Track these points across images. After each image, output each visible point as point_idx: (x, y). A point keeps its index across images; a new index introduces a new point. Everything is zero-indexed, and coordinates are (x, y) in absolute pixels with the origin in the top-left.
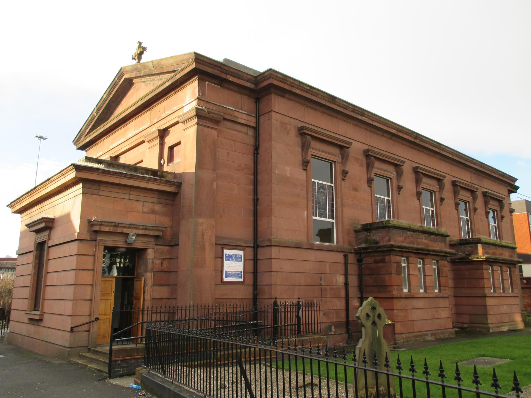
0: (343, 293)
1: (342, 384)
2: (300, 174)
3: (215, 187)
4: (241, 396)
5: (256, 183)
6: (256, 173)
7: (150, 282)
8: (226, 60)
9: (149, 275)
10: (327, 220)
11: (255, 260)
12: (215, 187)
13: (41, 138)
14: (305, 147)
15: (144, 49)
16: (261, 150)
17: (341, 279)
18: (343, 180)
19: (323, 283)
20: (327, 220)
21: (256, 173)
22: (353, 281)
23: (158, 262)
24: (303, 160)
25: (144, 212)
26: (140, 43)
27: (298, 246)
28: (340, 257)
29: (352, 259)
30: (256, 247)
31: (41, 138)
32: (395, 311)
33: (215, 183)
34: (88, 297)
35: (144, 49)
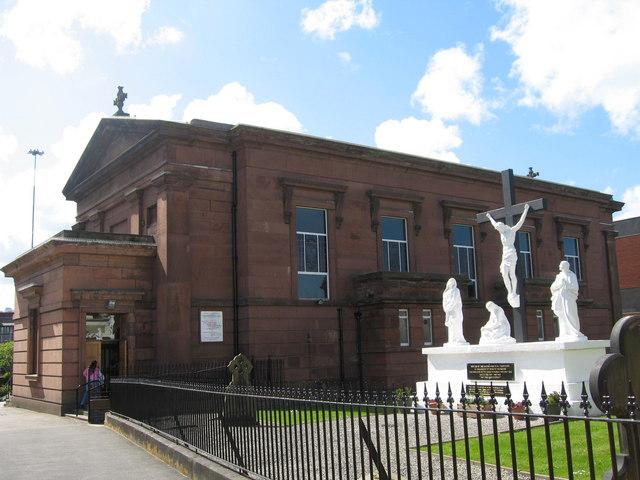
0: (337, 349)
1: (525, 475)
2: (283, 229)
3: (188, 250)
4: (334, 478)
5: (234, 241)
6: (235, 232)
7: (132, 344)
8: (194, 120)
9: (132, 338)
10: (318, 273)
11: (236, 320)
12: (188, 250)
13: (35, 153)
14: (286, 198)
15: (125, 96)
16: (239, 207)
17: (334, 335)
18: (338, 228)
19: (310, 339)
20: (318, 273)
21: (235, 232)
22: (350, 335)
23: (140, 325)
24: (285, 212)
25: (123, 278)
26: (120, 88)
27: (278, 303)
28: (333, 312)
29: (349, 313)
30: (236, 307)
31: (35, 153)
32: (388, 366)
33: (188, 247)
34: (75, 360)
35: (125, 96)
